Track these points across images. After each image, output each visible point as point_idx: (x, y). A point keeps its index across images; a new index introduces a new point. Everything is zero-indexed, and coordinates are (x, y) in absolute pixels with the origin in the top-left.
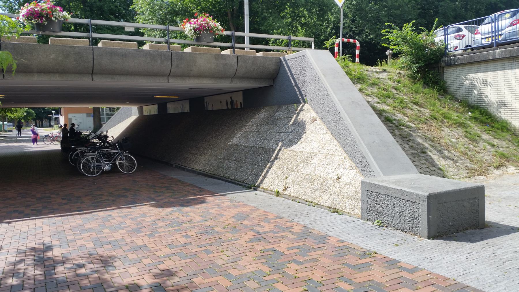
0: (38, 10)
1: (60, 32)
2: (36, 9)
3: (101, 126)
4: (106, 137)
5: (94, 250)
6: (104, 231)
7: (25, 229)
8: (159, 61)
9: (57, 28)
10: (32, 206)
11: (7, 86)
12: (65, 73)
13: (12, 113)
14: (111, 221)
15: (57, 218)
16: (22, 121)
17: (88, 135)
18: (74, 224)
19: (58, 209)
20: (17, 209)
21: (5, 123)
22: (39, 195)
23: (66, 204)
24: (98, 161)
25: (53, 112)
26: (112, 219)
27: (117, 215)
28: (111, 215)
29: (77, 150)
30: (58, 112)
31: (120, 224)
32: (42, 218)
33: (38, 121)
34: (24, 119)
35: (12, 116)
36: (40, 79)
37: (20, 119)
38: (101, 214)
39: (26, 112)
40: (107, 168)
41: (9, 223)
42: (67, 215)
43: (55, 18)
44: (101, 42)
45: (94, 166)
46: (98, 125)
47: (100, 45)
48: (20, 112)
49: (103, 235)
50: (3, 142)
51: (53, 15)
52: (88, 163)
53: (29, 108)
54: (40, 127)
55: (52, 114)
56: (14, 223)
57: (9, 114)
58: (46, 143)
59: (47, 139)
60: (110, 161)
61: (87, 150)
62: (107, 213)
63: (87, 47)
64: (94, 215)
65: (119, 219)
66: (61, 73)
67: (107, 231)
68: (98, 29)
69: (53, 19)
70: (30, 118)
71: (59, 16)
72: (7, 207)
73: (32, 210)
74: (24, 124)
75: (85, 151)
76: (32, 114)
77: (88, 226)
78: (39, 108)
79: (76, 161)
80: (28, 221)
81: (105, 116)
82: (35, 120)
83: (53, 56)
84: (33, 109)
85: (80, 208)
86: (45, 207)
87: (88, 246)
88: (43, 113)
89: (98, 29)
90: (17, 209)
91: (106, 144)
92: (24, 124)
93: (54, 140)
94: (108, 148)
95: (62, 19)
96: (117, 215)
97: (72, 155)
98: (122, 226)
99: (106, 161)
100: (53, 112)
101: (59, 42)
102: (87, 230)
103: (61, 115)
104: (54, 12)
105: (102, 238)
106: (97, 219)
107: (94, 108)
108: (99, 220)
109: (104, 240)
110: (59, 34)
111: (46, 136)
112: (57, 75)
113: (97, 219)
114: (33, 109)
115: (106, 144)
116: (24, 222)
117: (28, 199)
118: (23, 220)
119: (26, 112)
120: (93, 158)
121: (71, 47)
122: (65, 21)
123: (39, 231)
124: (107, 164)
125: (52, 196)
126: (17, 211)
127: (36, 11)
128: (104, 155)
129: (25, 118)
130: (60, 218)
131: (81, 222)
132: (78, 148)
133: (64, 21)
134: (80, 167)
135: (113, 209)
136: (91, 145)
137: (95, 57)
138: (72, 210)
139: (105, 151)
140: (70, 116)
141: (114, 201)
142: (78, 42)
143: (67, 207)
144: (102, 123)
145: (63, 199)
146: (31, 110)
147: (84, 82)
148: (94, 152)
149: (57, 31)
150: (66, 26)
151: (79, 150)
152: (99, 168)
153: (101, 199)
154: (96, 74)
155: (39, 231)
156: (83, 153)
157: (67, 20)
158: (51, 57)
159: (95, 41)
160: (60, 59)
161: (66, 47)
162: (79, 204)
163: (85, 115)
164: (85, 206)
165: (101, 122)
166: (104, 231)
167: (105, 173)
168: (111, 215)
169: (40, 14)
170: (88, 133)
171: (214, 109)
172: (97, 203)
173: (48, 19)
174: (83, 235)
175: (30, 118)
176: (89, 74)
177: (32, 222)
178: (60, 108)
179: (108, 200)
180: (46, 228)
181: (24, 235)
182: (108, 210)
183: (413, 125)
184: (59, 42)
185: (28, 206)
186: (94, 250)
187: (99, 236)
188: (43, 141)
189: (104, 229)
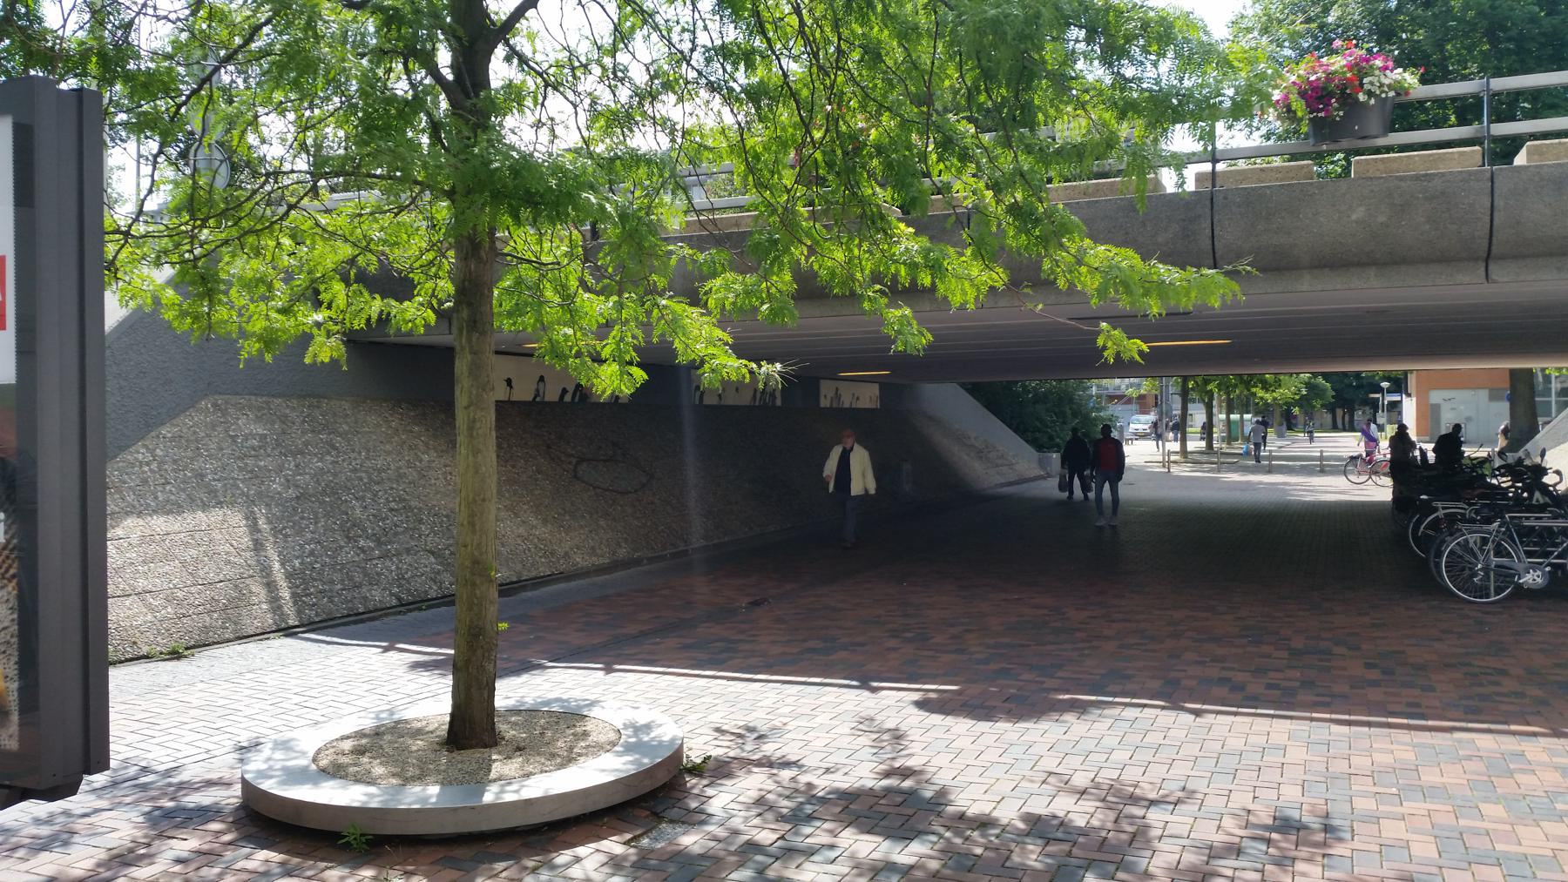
0: (1318, 79)
1: (1385, 134)
2: (1313, 78)
3: (1533, 431)
4: (1541, 471)
5: (1435, 870)
6: (1487, 809)
7: (1235, 743)
8: (876, 29)
9: (1374, 123)
10: (1272, 674)
11: (1248, 314)
12: (1396, 263)
13: (1267, 390)
14: (1520, 778)
15: (1335, 728)
16: (1296, 411)
17: (1484, 462)
18: (1386, 759)
19: (1345, 697)
20: (1229, 674)
21: (1247, 416)
22: (1298, 643)
23: (1375, 684)
24: (1500, 552)
25: (1385, 385)
26: (1523, 771)
27: (1545, 758)
28: (1522, 754)
29: (1436, 510)
30: (1399, 385)
31: (1552, 796)
32: (1291, 718)
33: (1339, 412)
34: (1301, 407)
35: (1268, 397)
36: (1320, 287)
37: (1289, 404)
38: (1486, 743)
39: (1308, 385)
40: (1533, 578)
41: (1197, 713)
42: (1369, 724)
43: (1370, 94)
44: (1524, 151)
45: (1486, 569)
46: (1523, 429)
47: (1520, 159)
48: (1291, 385)
49: (1478, 824)
50: (1235, 471)
51: (1362, 85)
52: (1468, 557)
53: (1315, 375)
54: (1344, 430)
55: (1381, 390)
56: (1210, 718)
57: (1261, 393)
58: (1352, 478)
59: (1334, 471)
60: (1547, 555)
61: (1469, 512)
62: (1509, 744)
63: (1470, 173)
64: (1459, 741)
65: (1552, 778)
66: (1385, 264)
67: (1493, 810)
68: (1507, 106)
69: (1362, 97)
70: (1317, 404)
71: (1382, 85)
72: (1203, 663)
73: (1269, 686)
74: (1301, 419)
75: (1463, 515)
76: (1325, 390)
77: (1430, 777)
78: (1345, 374)
79: (1432, 544)
80: (1250, 719)
81: (1553, 398)
82: (1331, 409)
83: (1359, 213)
84: (1326, 376)
85: (1418, 705)
86: (1308, 684)
87: (1416, 849)
88: (1358, 387)
89: (1507, 106)
90: (1229, 674)
91: (1537, 495)
92: (1301, 419)
93: (1376, 473)
94: (1542, 508)
95: (1392, 94)
96: (1545, 758)
97: (1419, 522)
98: (1559, 806)
99: (1529, 554)
100: (1385, 385)
101: (1381, 167)
102: (1426, 793)
103: (1409, 395)
104: (1367, 75)
105: (1476, 832)
106: (1469, 758)
107: (1513, 372)
108: (1479, 766)
109: (1478, 844)
110: (1381, 142)
111: (1353, 458)
112: (1372, 271)
113: (1469, 758)
114: (1326, 376)
115: (1537, 495)
116: (1238, 719)
117: (1266, 649)
118: (1235, 714)
119: (1308, 385)
120: (1485, 541)
121: (1417, 178)
122: (1403, 98)
123: (1273, 758)
124: (1535, 566)
125: (1337, 650)
126: (1228, 680)
127: (1310, 83)
128: (1526, 534)
129: (1304, 402)
130: (1345, 729)
131: (1409, 756)
132: (1439, 504)
133: (1398, 100)
134: (1438, 565)
135: (1535, 734)
136: (1482, 497)
137: (1499, 202)
138: (1391, 708)
139: (1531, 521)
140: (1436, 397)
141: (1544, 702)
142: (1441, 158)
143: (1375, 694)
144: (1541, 420)
145: (1369, 666)
146: (1320, 380)
147: (1463, 288)
148: (1489, 521)
149: (1374, 133)
150: (1405, 114)
151: (1442, 509)
152: (1506, 576)
153: (1497, 689)
154: (1503, 258)
155: (1273, 758)
156: (1451, 519)
157: (1407, 93)
158: (1354, 217)
159: (1506, 149)
160: (1382, 219)
161: (1401, 179)
162: (1417, 692)
163: (1484, 394)
164: (1437, 704)
165: (1534, 416)
166: (1487, 809)
167: (1522, 593)
168: (1522, 754)
169: (1324, 88)
170: (1482, 453)
171: (514, 398)
172: (1481, 702)
173: (1348, 100)
174: (1408, 807)
175: (1317, 404)
176: (1476, 259)
177: (1262, 724)
178: (1406, 373)
179: (1522, 695)
180: (1297, 754)
181: (1229, 762)
182: (1514, 733)
183: (1101, 253)
184: (1381, 167)
185: (1259, 672)
186: (1435, 870)
187: (1462, 822)
188: (1345, 473)
189: (1486, 800)
